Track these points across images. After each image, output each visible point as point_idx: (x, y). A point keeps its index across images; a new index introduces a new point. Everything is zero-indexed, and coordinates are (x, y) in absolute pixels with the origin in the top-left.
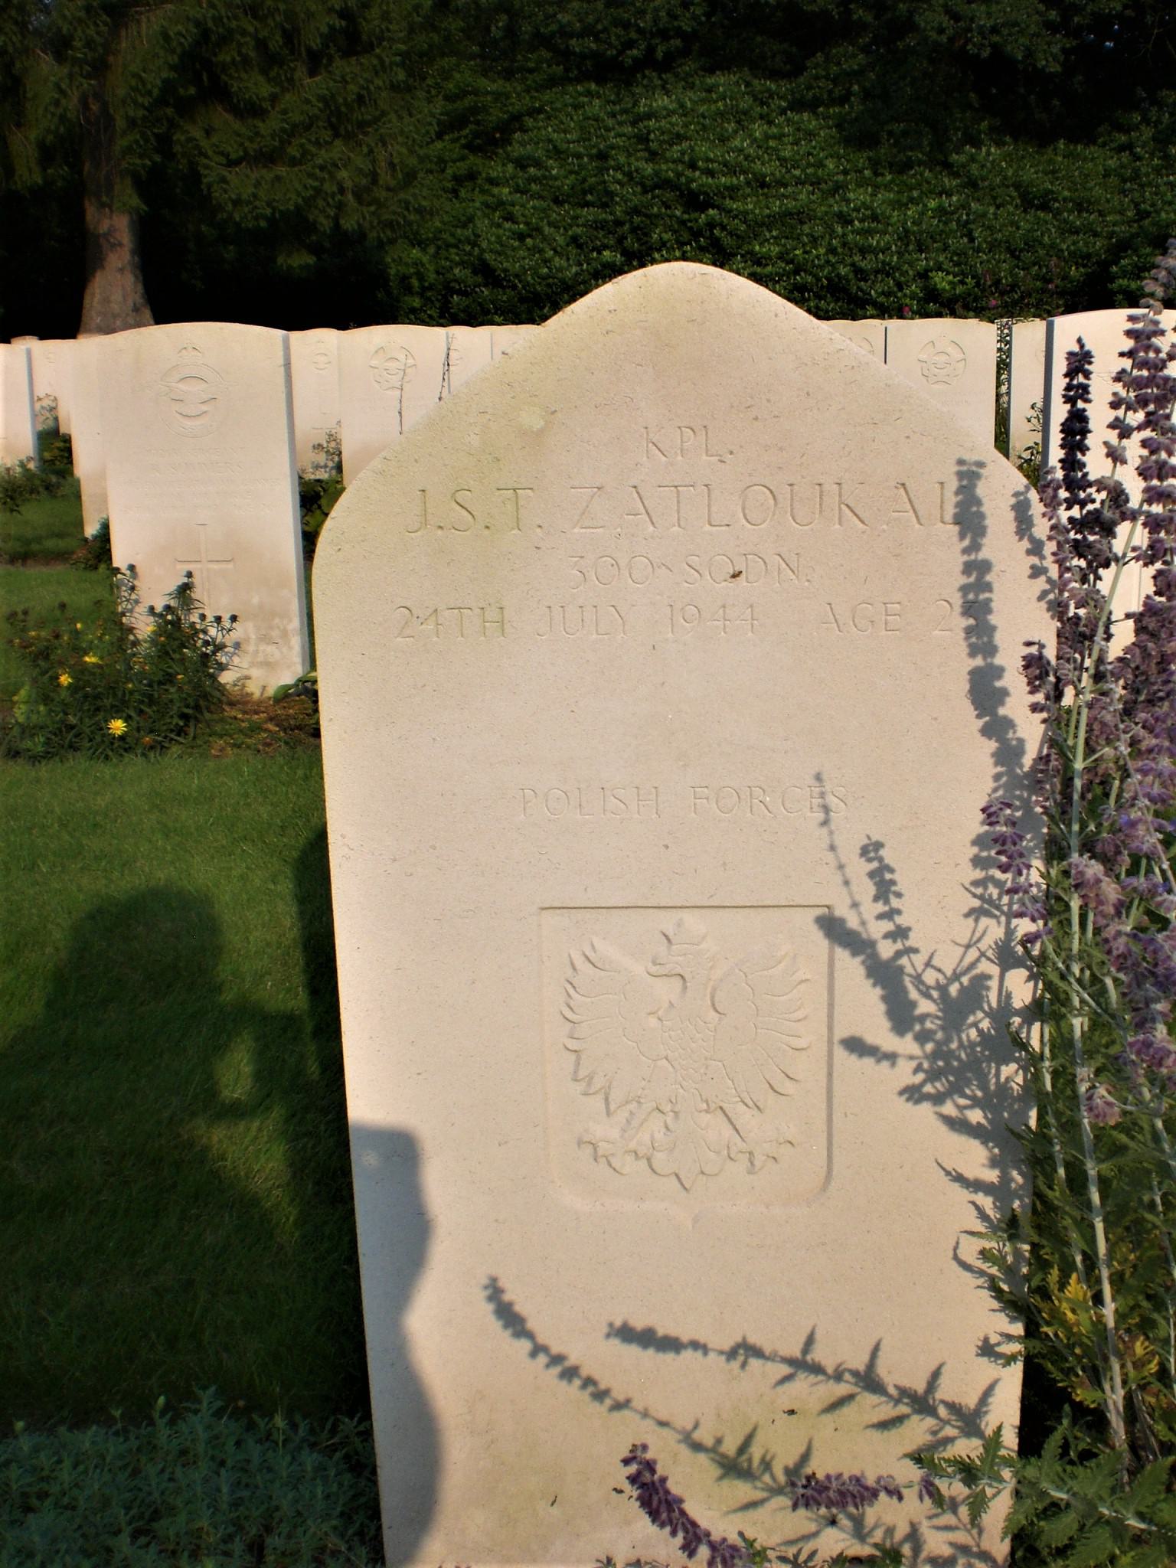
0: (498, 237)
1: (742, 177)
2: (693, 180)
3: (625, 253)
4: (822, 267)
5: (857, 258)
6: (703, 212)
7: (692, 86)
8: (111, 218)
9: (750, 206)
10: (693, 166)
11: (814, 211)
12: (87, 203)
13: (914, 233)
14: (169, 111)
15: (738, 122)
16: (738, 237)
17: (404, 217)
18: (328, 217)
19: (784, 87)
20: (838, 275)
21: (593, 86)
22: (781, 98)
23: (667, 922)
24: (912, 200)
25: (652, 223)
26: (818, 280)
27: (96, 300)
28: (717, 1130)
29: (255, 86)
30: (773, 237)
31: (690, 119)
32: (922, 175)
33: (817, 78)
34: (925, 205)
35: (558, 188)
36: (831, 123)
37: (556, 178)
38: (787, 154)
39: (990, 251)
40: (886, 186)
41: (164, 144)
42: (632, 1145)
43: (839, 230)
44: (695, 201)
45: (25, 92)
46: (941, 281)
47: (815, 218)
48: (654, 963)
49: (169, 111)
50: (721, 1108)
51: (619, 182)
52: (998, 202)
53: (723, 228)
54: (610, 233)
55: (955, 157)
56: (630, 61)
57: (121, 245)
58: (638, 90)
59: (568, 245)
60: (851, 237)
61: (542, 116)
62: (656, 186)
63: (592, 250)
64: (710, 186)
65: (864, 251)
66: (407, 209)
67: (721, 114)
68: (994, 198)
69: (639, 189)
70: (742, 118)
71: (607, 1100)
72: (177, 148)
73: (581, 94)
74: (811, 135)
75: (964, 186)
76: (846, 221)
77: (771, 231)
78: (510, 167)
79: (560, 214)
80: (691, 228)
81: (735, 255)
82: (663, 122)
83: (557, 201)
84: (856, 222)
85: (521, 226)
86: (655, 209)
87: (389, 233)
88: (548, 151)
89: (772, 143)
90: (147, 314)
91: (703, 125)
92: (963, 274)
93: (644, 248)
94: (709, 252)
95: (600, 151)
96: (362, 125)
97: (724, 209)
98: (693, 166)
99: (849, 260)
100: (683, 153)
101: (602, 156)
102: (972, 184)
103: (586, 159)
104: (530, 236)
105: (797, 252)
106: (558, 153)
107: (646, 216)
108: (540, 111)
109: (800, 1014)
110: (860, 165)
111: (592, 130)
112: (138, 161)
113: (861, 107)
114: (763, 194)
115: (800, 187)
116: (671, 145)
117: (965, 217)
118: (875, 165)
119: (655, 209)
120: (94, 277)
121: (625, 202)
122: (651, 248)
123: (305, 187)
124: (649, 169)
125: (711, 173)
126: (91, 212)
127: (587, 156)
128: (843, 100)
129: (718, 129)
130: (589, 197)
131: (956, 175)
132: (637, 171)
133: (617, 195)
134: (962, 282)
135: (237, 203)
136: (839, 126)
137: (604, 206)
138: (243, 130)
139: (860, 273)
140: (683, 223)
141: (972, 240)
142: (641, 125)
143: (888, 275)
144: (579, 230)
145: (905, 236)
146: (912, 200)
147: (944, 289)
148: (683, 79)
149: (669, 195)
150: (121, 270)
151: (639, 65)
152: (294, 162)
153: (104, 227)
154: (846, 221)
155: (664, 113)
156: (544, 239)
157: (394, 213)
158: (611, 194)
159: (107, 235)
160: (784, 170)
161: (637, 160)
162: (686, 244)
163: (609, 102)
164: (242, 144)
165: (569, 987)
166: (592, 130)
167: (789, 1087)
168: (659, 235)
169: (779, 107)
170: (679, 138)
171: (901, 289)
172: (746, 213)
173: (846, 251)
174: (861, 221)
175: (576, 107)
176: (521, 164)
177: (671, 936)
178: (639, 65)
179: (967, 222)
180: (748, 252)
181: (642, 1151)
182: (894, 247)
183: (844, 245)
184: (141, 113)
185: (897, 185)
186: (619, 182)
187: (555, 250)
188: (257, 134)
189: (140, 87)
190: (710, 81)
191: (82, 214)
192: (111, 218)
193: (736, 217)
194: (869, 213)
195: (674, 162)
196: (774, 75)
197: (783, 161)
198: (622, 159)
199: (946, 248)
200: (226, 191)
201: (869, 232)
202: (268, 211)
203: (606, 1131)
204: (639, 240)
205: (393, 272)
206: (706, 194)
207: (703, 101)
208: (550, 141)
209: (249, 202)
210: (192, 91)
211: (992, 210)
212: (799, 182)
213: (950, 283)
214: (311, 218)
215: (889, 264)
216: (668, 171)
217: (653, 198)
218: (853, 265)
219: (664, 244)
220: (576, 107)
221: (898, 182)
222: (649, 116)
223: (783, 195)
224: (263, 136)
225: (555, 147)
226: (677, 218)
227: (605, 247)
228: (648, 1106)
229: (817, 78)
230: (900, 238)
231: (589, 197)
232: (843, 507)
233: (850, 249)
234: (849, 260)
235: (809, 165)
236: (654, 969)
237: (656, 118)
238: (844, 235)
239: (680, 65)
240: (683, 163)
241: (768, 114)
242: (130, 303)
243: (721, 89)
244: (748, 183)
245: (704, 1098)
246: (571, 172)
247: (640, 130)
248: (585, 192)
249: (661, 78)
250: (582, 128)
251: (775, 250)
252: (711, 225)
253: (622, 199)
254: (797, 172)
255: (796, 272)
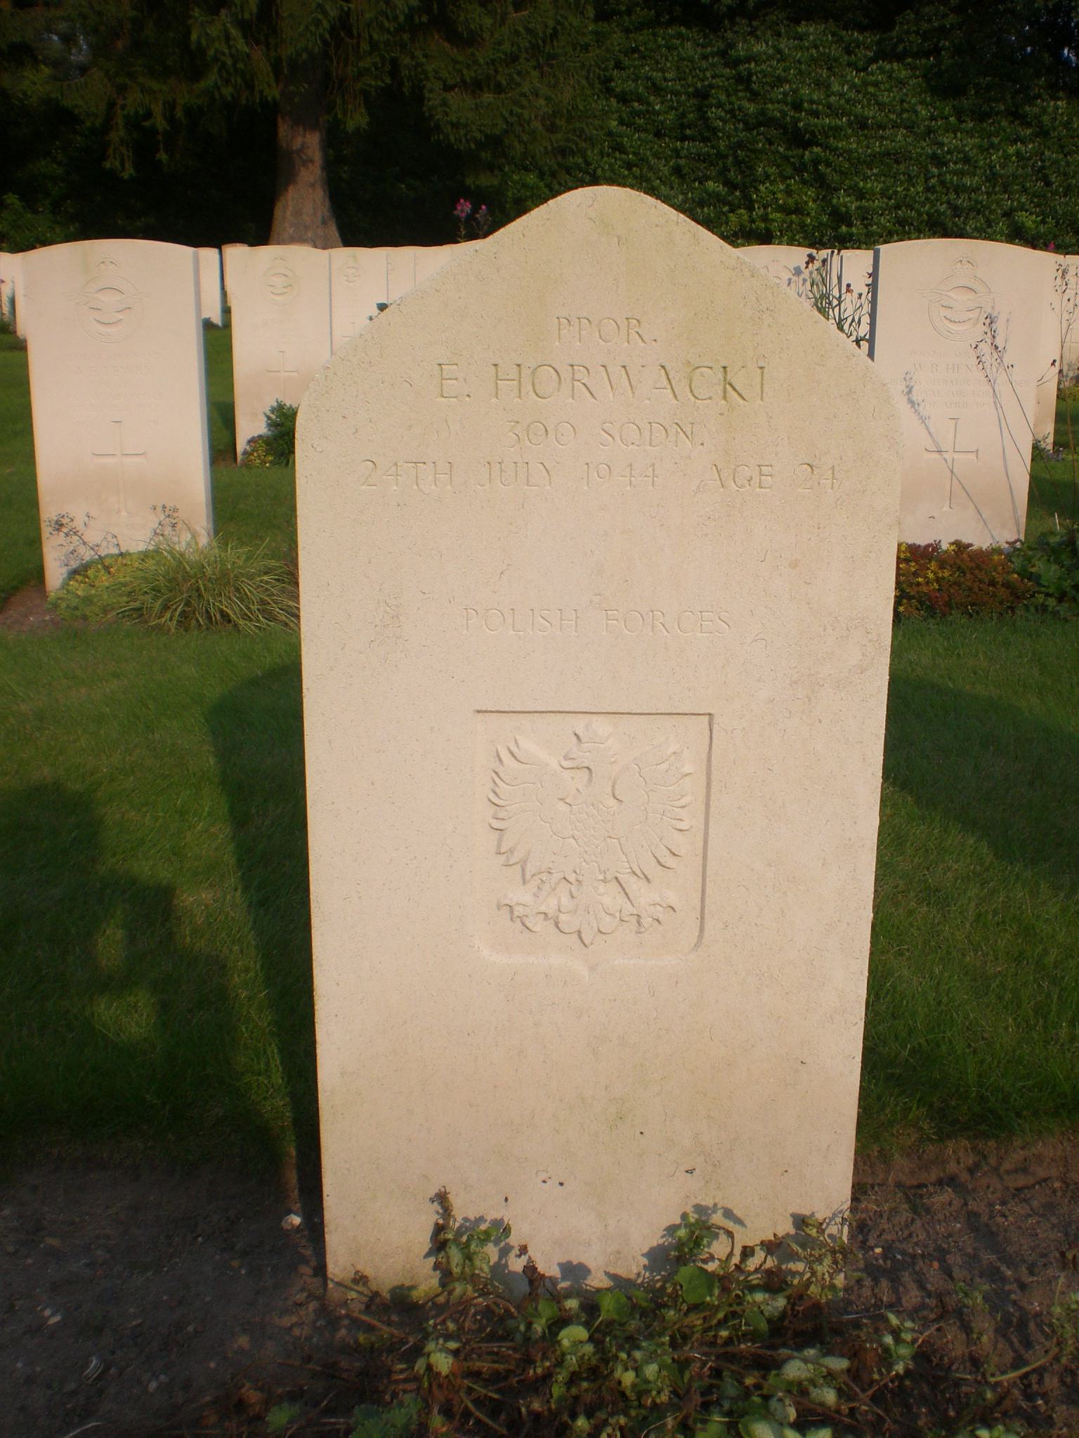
0: (610, 165)
1: (844, 119)
2: (799, 120)
3: (727, 183)
4: (923, 204)
5: (953, 196)
6: (805, 148)
7: (779, 35)
8: (304, 136)
9: (854, 146)
10: (797, 107)
11: (910, 152)
12: (280, 121)
13: (1001, 176)
14: (406, 36)
15: (829, 69)
16: (841, 173)
17: (576, 144)
18: (520, 142)
19: (869, 38)
20: (937, 211)
21: (683, 30)
22: (867, 48)
23: (579, 724)
24: (992, 146)
25: (757, 158)
26: (920, 214)
27: (288, 213)
28: (610, 897)
29: (475, 17)
30: (873, 174)
31: (788, 64)
32: (999, 124)
33: (908, 32)
34: (1004, 151)
35: (662, 123)
36: (918, 73)
37: (658, 113)
38: (886, 100)
39: (1065, 195)
40: (967, 132)
41: (395, 66)
42: (543, 909)
43: (935, 171)
44: (799, 139)
45: (277, 13)
46: (1028, 221)
47: (911, 159)
48: (566, 758)
49: (406, 36)
50: (616, 878)
51: (721, 119)
52: (1066, 150)
53: (828, 164)
54: (712, 165)
55: (1027, 108)
56: (725, 9)
57: (312, 161)
58: (729, 35)
59: (671, 175)
60: (948, 177)
61: (636, 56)
62: (761, 124)
63: (695, 181)
64: (816, 125)
65: (958, 190)
66: (580, 137)
67: (812, 59)
68: (1062, 147)
69: (741, 126)
70: (831, 64)
71: (523, 870)
72: (405, 72)
73: (672, 37)
74: (902, 83)
75: (1037, 135)
76: (938, 161)
77: (871, 169)
78: (613, 101)
79: (661, 146)
80: (793, 164)
81: (836, 190)
82: (763, 67)
83: (658, 135)
84: (951, 164)
85: (631, 156)
86: (760, 145)
87: (560, 158)
88: (647, 88)
89: (871, 89)
90: (333, 231)
91: (800, 70)
92: (1043, 213)
93: (747, 180)
94: (811, 185)
95: (697, 90)
96: (552, 57)
97: (827, 147)
98: (797, 107)
99: (945, 199)
100: (785, 94)
101: (702, 95)
102: (1043, 133)
103: (683, 97)
104: (636, 166)
105: (899, 189)
106: (656, 89)
107: (751, 151)
108: (634, 50)
109: (683, 802)
110: (946, 112)
111: (687, 71)
112: (373, 83)
113: (950, 61)
114: (862, 135)
115: (896, 130)
116: (772, 88)
117: (1039, 163)
118: (959, 114)
119: (760, 145)
120: (287, 191)
121: (728, 137)
122: (755, 181)
123: (511, 113)
124: (752, 108)
125: (816, 114)
126: (283, 130)
127: (685, 93)
128: (936, 51)
129: (813, 74)
130: (688, 132)
131: (1029, 125)
132: (740, 109)
133: (720, 131)
134: (1043, 222)
135: (455, 126)
136: (924, 76)
137: (705, 140)
138: (461, 58)
139: (956, 211)
140: (786, 158)
141: (1048, 184)
142: (741, 68)
143: (978, 212)
144: (682, 162)
145: (992, 178)
146: (992, 146)
147: (1030, 228)
148: (770, 28)
149: (773, 132)
150: (313, 185)
151: (732, 13)
152: (499, 89)
153: (297, 144)
154: (938, 161)
155: (764, 57)
156: (650, 168)
157: (568, 140)
158: (714, 130)
159: (301, 150)
160: (883, 114)
161: (739, 99)
162: (790, 178)
163: (698, 45)
164: (460, 71)
165: (494, 775)
166: (687, 71)
167: (670, 861)
168: (763, 169)
169: (865, 56)
170: (780, 81)
171: (990, 226)
172: (850, 151)
173: (944, 191)
174: (955, 163)
175: (670, 48)
176: (624, 99)
177: (581, 735)
178: (732, 13)
179: (1043, 168)
180: (850, 188)
181: (551, 913)
182: (983, 188)
183: (942, 183)
184: (386, 36)
185: (978, 132)
186: (721, 119)
187: (660, 179)
188: (476, 62)
189: (389, 13)
190: (801, 29)
191: (274, 126)
192: (304, 136)
193: (841, 155)
194: (961, 156)
195: (778, 102)
196: (862, 29)
197: (881, 106)
198: (723, 97)
199: (1025, 190)
200: (447, 114)
201: (961, 173)
202: (478, 135)
203: (521, 896)
204: (742, 172)
205: (510, 194)
206: (813, 133)
207: (795, 48)
208: (648, 79)
209: (466, 125)
210: (425, 19)
211: (1061, 156)
212: (896, 126)
213: (1034, 222)
214: (507, 142)
215: (981, 202)
216: (773, 110)
217: (758, 134)
218: (948, 203)
219: (768, 177)
220: (670, 48)
221: (978, 129)
222: (749, 60)
223: (882, 137)
224: (480, 65)
225: (654, 84)
226: (780, 153)
227: (708, 178)
228: (556, 876)
229: (908, 32)
230: (988, 180)
231: (688, 132)
232: (728, 386)
233: (948, 189)
234: (945, 199)
235: (903, 111)
236: (565, 764)
237: (756, 62)
238: (940, 175)
239: (767, 14)
240: (786, 104)
241: (856, 63)
242: (319, 215)
243: (811, 37)
244: (850, 124)
245: (609, 877)
246: (672, 108)
247: (739, 74)
248: (682, 126)
249: (750, 25)
250: (678, 68)
251: (878, 187)
252: (816, 162)
253: (724, 134)
254: (893, 117)
255: (898, 207)
